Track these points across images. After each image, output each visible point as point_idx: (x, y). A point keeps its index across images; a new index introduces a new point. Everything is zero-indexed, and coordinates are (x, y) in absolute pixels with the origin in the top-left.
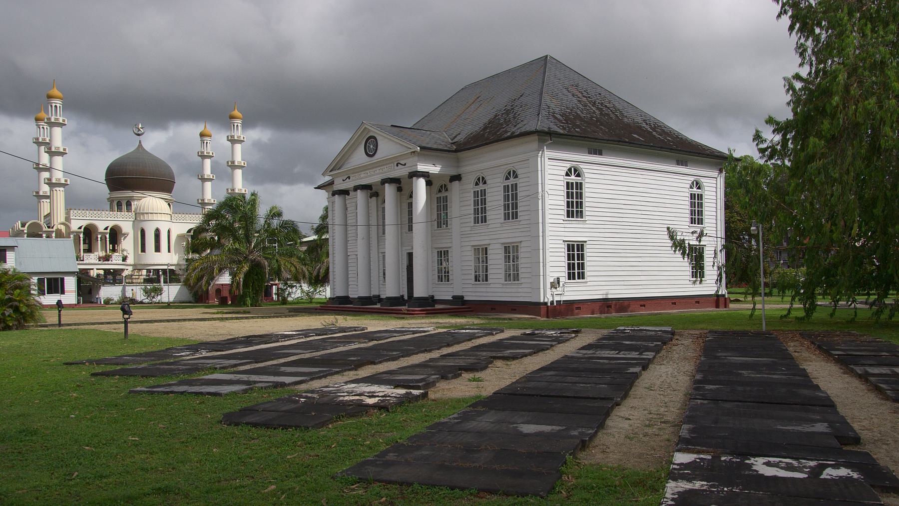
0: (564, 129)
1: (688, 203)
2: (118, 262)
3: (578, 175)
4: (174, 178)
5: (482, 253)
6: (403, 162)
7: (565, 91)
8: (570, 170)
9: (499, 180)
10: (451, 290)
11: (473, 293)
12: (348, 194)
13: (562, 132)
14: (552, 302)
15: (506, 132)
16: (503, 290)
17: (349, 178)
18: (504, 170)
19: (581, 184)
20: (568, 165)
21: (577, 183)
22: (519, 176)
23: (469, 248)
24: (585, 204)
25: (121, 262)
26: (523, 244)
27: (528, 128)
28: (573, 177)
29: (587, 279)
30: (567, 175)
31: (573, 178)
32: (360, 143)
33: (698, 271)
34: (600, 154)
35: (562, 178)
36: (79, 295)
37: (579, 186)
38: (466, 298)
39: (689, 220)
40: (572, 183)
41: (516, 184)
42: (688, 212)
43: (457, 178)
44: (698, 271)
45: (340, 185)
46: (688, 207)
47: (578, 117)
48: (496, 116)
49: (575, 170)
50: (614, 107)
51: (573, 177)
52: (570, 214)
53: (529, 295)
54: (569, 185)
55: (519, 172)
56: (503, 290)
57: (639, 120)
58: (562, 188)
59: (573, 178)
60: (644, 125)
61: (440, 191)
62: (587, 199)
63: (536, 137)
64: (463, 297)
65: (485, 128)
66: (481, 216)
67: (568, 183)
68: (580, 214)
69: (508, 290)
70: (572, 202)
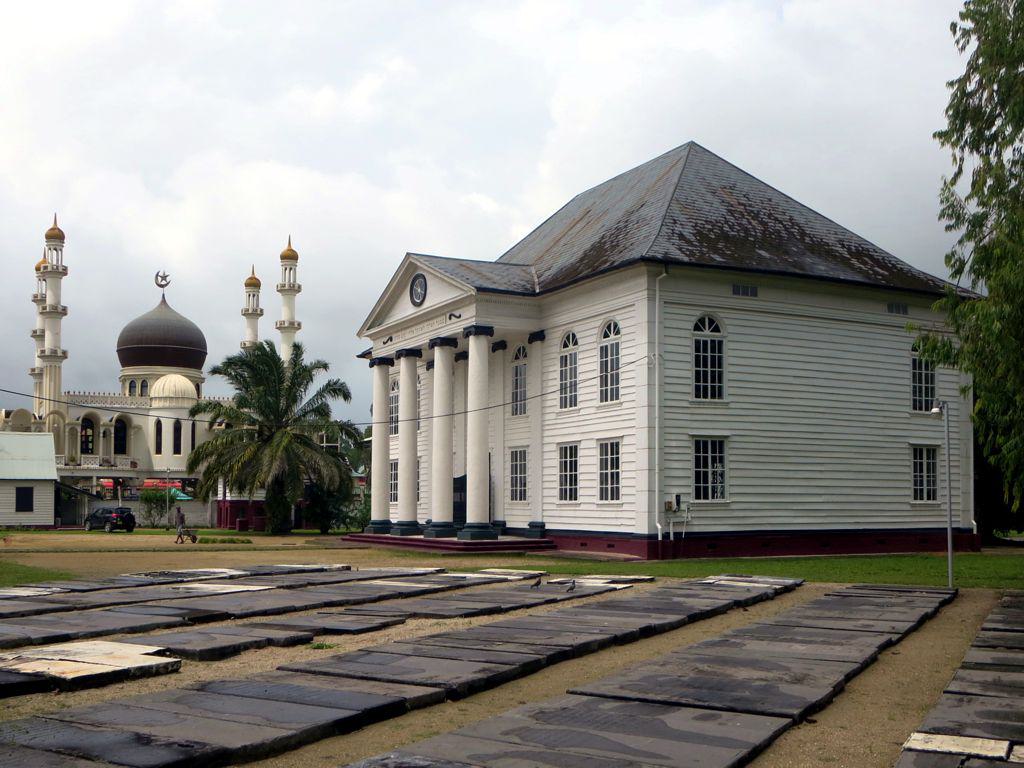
0: (692, 254)
1: (909, 375)
2: (124, 467)
3: (717, 329)
4: (204, 346)
5: (569, 454)
6: (457, 313)
7: (709, 197)
8: (702, 321)
9: (594, 339)
10: (528, 513)
11: (562, 518)
12: (392, 365)
13: (686, 259)
14: (666, 536)
15: (605, 262)
16: (597, 514)
17: (391, 339)
18: (599, 322)
19: (720, 343)
20: (698, 313)
21: (713, 342)
22: (623, 332)
23: (594, 444)
24: (726, 362)
25: (128, 467)
26: (626, 441)
27: (628, 256)
28: (707, 332)
29: (580, 500)
30: (697, 328)
31: (707, 334)
32: (405, 287)
33: (924, 488)
34: (754, 294)
35: (687, 334)
36: (56, 516)
37: (717, 346)
38: (547, 527)
39: (691, 389)
40: (705, 342)
41: (617, 344)
42: (910, 389)
43: (538, 336)
44: (924, 488)
45: (381, 352)
46: (910, 382)
47: (725, 237)
48: (603, 238)
49: (711, 322)
50: (791, 219)
51: (707, 332)
52: (699, 392)
53: (633, 522)
54: (699, 346)
55: (621, 325)
56: (597, 514)
57: (831, 239)
58: (688, 350)
59: (707, 334)
60: (839, 248)
61: (517, 358)
62: (941, 385)
63: (643, 268)
64: (504, 523)
65: (582, 260)
66: (569, 400)
67: (697, 342)
68: (717, 393)
69: (603, 515)
70: (705, 373)
